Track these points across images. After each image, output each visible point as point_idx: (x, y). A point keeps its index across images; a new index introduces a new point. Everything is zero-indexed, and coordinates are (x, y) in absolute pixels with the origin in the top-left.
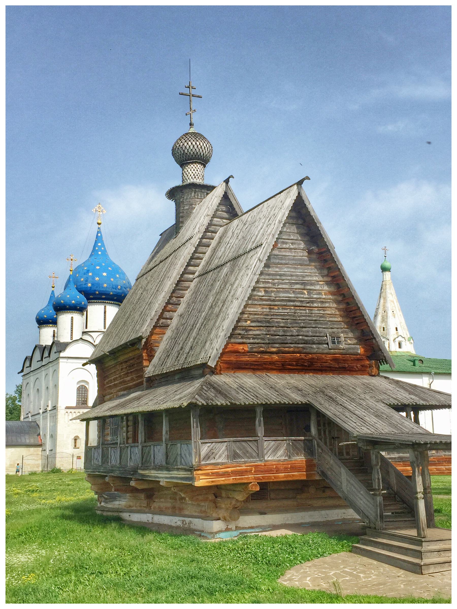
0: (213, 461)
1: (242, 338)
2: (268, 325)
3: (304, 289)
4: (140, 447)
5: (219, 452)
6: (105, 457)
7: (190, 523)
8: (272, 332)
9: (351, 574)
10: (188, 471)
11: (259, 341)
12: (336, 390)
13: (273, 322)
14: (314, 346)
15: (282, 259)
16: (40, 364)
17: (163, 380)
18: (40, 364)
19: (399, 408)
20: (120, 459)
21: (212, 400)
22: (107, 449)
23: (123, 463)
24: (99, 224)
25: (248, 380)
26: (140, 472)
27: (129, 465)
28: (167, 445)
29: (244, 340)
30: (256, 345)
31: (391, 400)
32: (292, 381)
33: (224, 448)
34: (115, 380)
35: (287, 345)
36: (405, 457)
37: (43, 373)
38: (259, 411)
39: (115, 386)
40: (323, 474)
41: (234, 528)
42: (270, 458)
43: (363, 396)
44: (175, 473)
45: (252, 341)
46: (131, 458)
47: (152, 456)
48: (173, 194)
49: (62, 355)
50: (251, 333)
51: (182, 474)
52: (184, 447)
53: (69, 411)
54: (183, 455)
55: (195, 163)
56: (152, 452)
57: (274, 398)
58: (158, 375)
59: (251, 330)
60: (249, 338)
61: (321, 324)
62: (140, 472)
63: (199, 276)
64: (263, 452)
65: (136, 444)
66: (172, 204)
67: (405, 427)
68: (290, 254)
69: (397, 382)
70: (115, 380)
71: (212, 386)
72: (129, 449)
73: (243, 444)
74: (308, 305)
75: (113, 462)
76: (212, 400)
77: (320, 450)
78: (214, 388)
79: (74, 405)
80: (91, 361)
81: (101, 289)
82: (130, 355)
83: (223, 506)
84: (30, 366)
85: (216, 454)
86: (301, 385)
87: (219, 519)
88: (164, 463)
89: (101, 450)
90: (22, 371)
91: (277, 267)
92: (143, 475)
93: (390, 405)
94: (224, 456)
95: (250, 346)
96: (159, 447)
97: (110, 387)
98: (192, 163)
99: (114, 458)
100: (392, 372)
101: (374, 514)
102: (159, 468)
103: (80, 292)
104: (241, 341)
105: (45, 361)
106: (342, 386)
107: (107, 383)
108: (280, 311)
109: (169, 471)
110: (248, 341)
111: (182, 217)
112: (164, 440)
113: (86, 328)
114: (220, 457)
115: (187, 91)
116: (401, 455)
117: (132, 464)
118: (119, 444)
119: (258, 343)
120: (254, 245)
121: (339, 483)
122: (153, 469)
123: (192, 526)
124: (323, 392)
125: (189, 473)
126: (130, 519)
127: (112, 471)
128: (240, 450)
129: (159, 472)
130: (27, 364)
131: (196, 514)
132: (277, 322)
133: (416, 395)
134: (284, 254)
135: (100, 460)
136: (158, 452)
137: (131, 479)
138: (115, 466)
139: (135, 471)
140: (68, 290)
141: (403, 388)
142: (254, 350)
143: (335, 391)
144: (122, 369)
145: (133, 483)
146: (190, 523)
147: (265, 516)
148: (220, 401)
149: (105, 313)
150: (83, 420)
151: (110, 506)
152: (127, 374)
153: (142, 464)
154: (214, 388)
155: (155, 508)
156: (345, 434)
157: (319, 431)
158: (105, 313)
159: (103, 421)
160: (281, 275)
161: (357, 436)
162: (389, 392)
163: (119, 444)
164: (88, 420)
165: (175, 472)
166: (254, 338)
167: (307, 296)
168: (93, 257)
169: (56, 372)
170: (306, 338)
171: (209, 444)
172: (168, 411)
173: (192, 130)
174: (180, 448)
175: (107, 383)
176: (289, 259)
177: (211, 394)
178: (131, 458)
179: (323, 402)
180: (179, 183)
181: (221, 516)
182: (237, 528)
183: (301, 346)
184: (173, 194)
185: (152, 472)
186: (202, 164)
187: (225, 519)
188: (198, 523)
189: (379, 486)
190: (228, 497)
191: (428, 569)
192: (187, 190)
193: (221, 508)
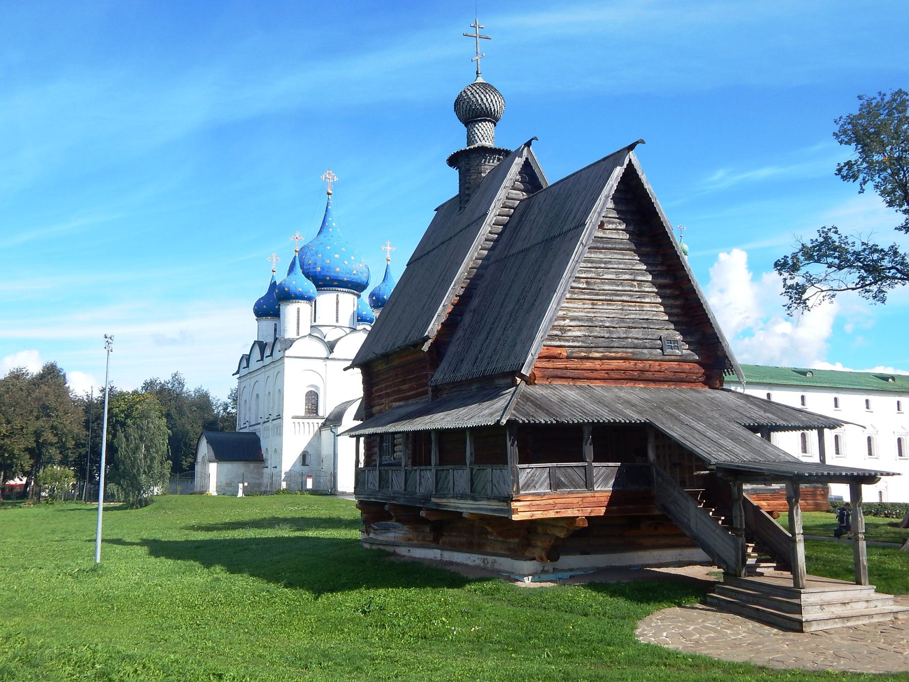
0: (532, 491)
1: (559, 340)
2: (590, 324)
3: (634, 280)
4: (434, 471)
5: (540, 479)
6: (383, 481)
7: (495, 562)
8: (596, 334)
9: (715, 631)
10: (504, 501)
11: (580, 344)
12: (676, 404)
13: (597, 320)
14: (645, 351)
15: (608, 243)
16: (261, 364)
17: (454, 390)
18: (261, 364)
19: (754, 429)
20: (406, 485)
21: (533, 416)
22: (387, 471)
23: (409, 490)
24: (329, 194)
25: (570, 393)
26: (434, 500)
27: (417, 491)
28: (472, 469)
29: (562, 343)
30: (577, 349)
31: (745, 419)
32: (622, 394)
33: (546, 474)
34: (386, 388)
35: (614, 350)
36: (759, 490)
37: (261, 377)
38: (586, 431)
39: (388, 395)
40: (665, 508)
41: (551, 570)
42: (599, 489)
43: (710, 413)
44: (483, 504)
45: (571, 344)
46: (420, 483)
47: (451, 482)
48: (454, 160)
49: (287, 353)
50: (569, 334)
51: (495, 505)
52: (497, 472)
53: (296, 421)
54: (495, 482)
55: (485, 121)
56: (451, 477)
57: (606, 416)
58: (447, 384)
59: (570, 330)
60: (568, 341)
61: (654, 324)
62: (434, 500)
63: (495, 262)
64: (592, 480)
65: (428, 467)
66: (454, 173)
67: (769, 453)
68: (617, 237)
69: (747, 397)
70: (386, 388)
71: (526, 398)
72: (418, 472)
73: (569, 470)
74: (638, 300)
75: (396, 488)
76: (533, 416)
77: (660, 479)
78: (532, 402)
79: (303, 414)
80: (352, 366)
81: (333, 274)
82: (409, 358)
83: (540, 544)
84: (248, 366)
85: (537, 483)
86: (632, 398)
87: (534, 559)
88: (468, 491)
89: (378, 472)
90: (238, 372)
91: (601, 253)
92: (437, 504)
93: (745, 426)
94: (546, 484)
95: (570, 350)
96: (460, 472)
97: (381, 397)
98: (481, 121)
99: (397, 482)
100: (739, 383)
101: (734, 559)
102: (463, 497)
103: (307, 275)
104: (558, 343)
105: (267, 361)
106: (682, 401)
107: (376, 392)
108: (605, 307)
109: (476, 500)
110: (567, 344)
111: (468, 189)
112: (468, 463)
113: (337, 321)
114: (541, 486)
115: (472, 32)
116: (755, 486)
117: (422, 490)
118: (403, 464)
119: (578, 347)
120: (573, 225)
121: (686, 520)
122: (453, 497)
123: (496, 566)
124: (662, 409)
125: (505, 504)
126: (409, 554)
127: (394, 498)
128: (566, 477)
129: (462, 501)
130: (244, 364)
131: (502, 552)
132: (601, 321)
133: (773, 414)
134: (609, 236)
135: (377, 485)
136: (460, 477)
137: (421, 509)
138: (399, 492)
139: (427, 499)
140: (292, 276)
141: (755, 404)
142: (575, 355)
143: (675, 408)
144: (396, 375)
145: (423, 514)
146: (495, 562)
147: (588, 556)
148: (542, 419)
149: (337, 303)
150: (352, 436)
151: (381, 538)
152: (404, 382)
153: (436, 491)
154: (532, 402)
155: (444, 543)
156: (702, 462)
157: (658, 456)
158: (337, 303)
159: (369, 438)
160: (605, 263)
161: (717, 463)
162: (740, 410)
163: (403, 464)
164: (358, 437)
165: (485, 502)
166: (573, 341)
167: (637, 289)
168: (322, 235)
169: (280, 374)
170: (636, 341)
171: (529, 470)
172: (472, 429)
173: (480, 80)
174: (489, 473)
175: (376, 392)
176: (615, 243)
177: (530, 408)
178: (420, 483)
179: (665, 421)
180: (464, 146)
181: (536, 556)
182: (555, 570)
183: (630, 350)
184: (454, 160)
185: (452, 501)
186: (492, 122)
187: (541, 559)
188: (505, 563)
189: (741, 525)
190: (547, 534)
191: (810, 626)
192: (474, 155)
193: (535, 547)
